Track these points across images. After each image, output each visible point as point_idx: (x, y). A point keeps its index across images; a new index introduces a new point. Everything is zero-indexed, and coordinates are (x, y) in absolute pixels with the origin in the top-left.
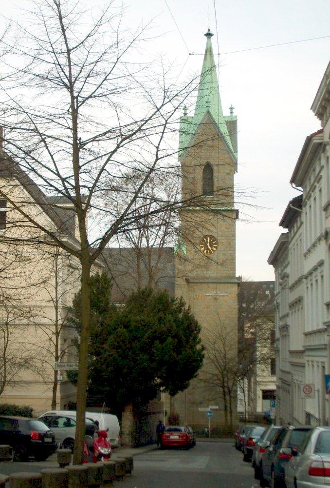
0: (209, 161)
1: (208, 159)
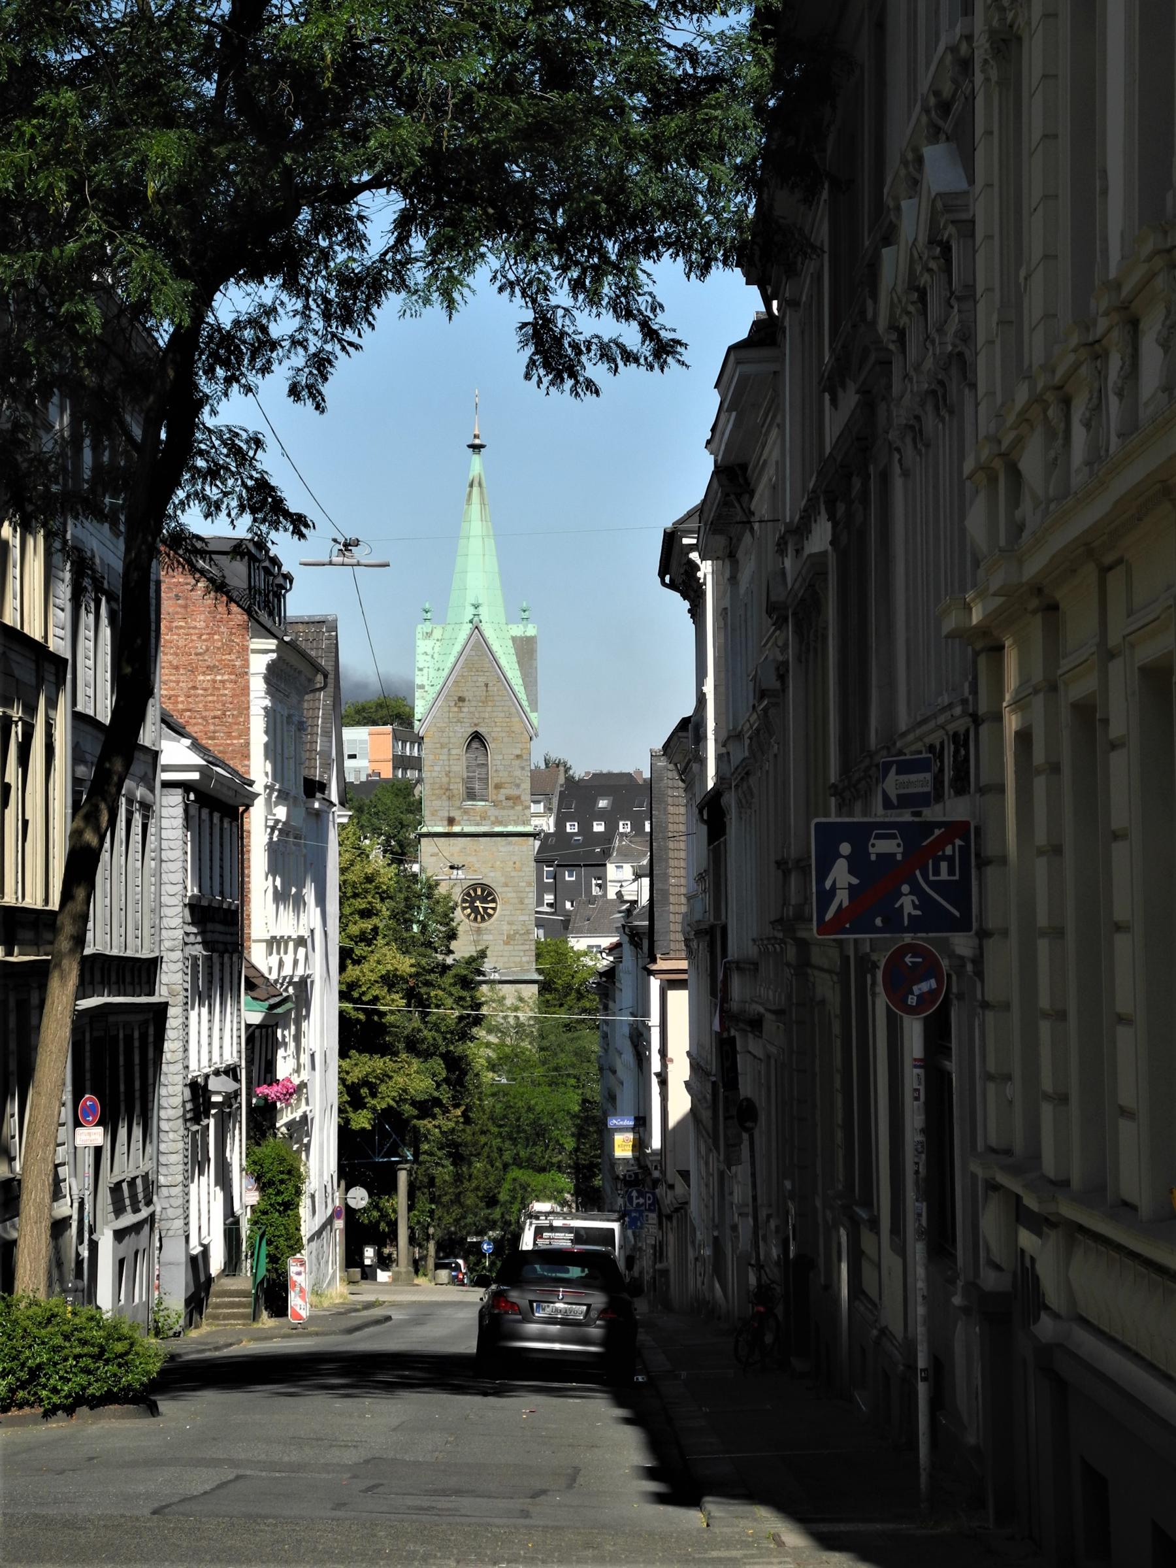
0: (480, 730)
1: (476, 725)
